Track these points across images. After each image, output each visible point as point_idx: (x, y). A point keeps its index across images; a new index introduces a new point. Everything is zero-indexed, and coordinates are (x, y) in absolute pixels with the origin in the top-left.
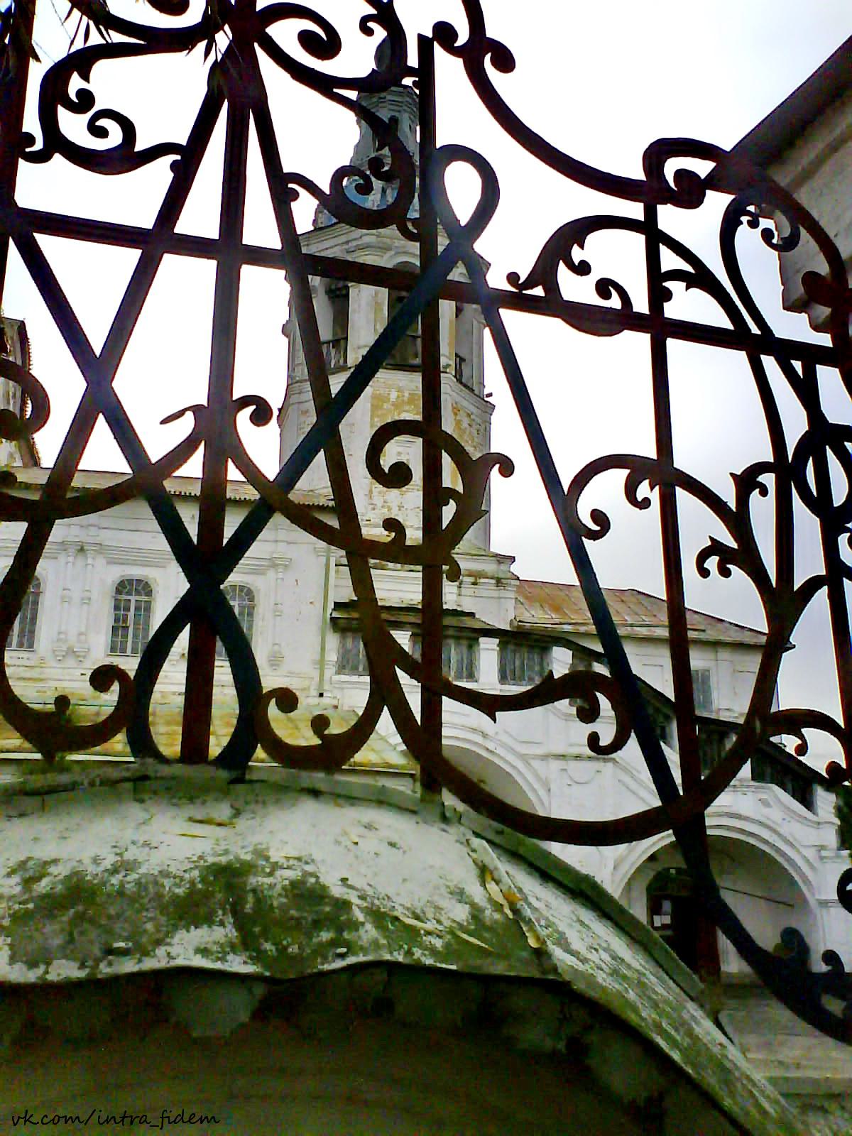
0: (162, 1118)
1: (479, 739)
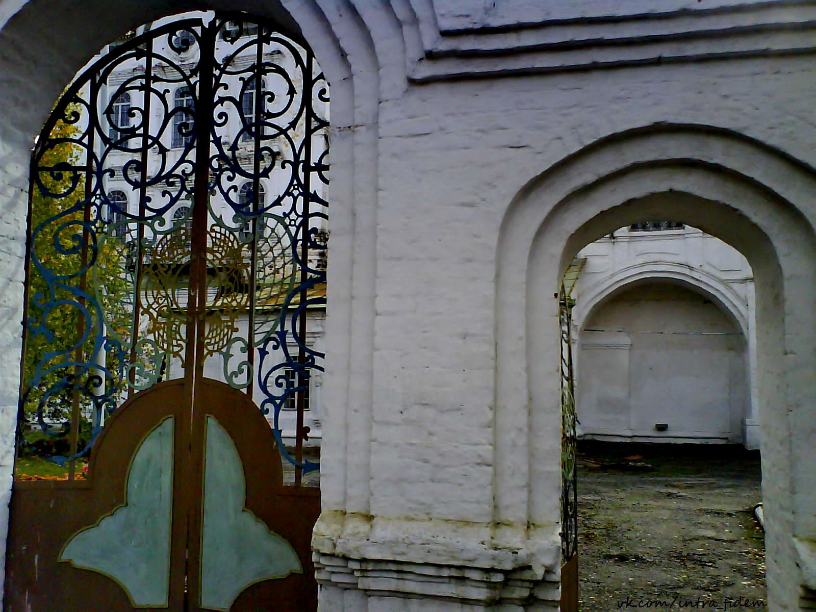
0: (726, 602)
1: (687, 271)
